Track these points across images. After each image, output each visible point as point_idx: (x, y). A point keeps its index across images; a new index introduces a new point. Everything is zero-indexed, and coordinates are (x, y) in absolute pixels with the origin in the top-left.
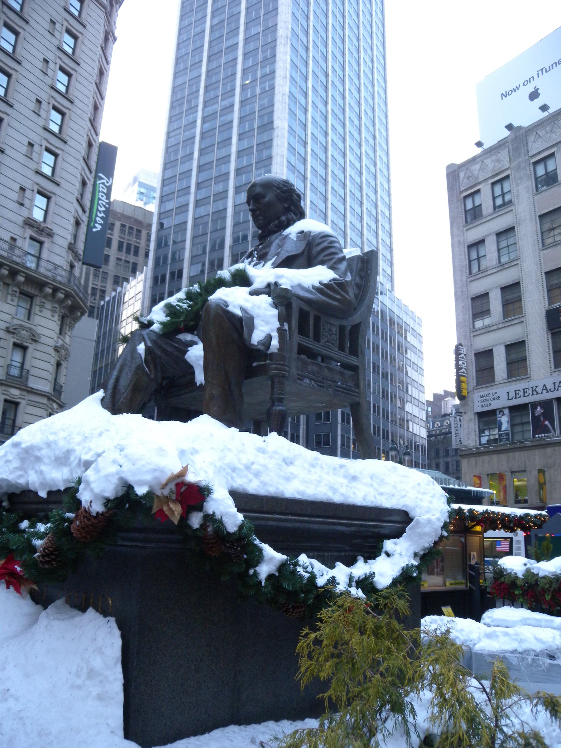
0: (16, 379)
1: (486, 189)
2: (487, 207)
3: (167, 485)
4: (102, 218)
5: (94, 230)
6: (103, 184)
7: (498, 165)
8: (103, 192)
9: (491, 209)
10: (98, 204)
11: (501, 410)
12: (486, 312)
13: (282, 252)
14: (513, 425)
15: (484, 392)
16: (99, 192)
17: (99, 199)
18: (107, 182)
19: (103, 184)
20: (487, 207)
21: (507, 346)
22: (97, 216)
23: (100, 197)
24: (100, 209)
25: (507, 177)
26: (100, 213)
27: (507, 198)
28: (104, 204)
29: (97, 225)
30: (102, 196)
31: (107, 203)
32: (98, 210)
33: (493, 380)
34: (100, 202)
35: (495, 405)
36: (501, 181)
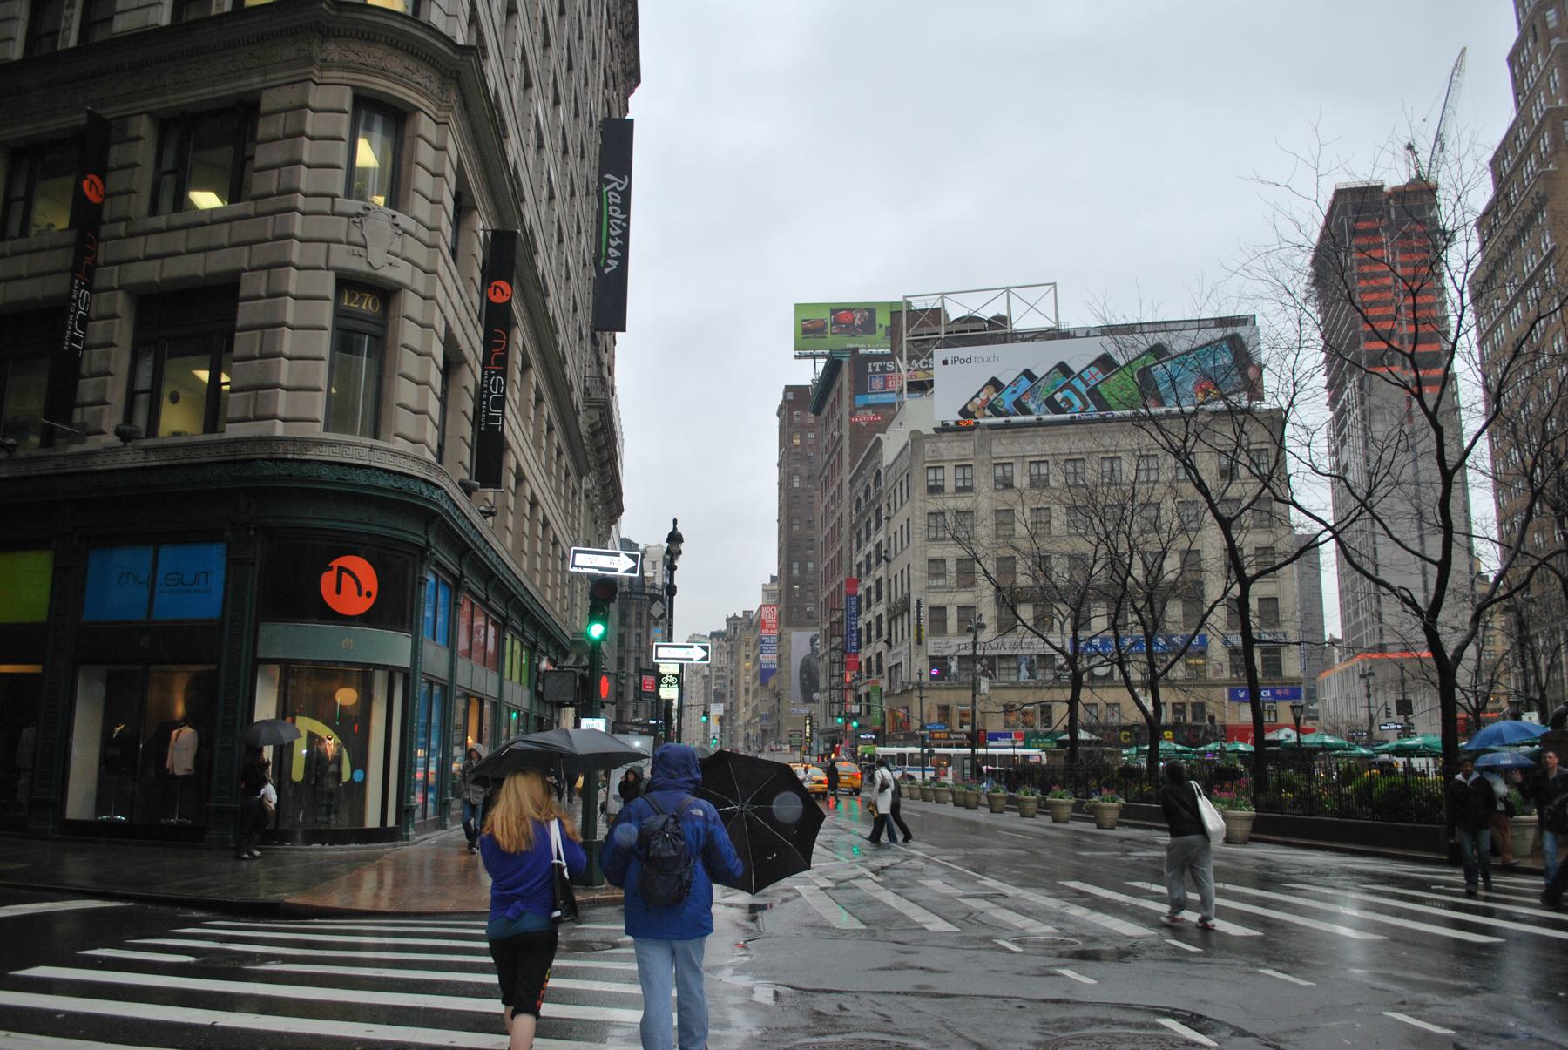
0: (132, 112)
1: (949, 469)
2: (950, 486)
3: (922, 968)
4: (617, 248)
5: (607, 271)
6: (614, 189)
7: (963, 452)
8: (614, 204)
9: (953, 489)
10: (609, 226)
11: (951, 658)
12: (942, 575)
13: (245, 863)
14: (960, 669)
15: (938, 640)
16: (609, 205)
17: (610, 217)
18: (621, 185)
19: (614, 189)
20: (950, 486)
21: (959, 608)
22: (609, 246)
23: (611, 213)
24: (613, 233)
25: (971, 466)
26: (614, 239)
27: (968, 484)
28: (619, 222)
29: (609, 261)
30: (614, 211)
31: (623, 220)
32: (609, 235)
33: (945, 632)
34: (611, 221)
35: (947, 652)
36: (964, 467)
